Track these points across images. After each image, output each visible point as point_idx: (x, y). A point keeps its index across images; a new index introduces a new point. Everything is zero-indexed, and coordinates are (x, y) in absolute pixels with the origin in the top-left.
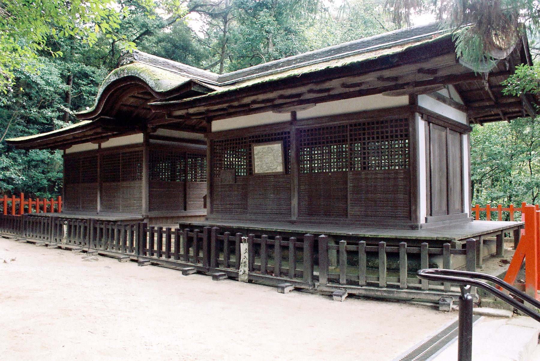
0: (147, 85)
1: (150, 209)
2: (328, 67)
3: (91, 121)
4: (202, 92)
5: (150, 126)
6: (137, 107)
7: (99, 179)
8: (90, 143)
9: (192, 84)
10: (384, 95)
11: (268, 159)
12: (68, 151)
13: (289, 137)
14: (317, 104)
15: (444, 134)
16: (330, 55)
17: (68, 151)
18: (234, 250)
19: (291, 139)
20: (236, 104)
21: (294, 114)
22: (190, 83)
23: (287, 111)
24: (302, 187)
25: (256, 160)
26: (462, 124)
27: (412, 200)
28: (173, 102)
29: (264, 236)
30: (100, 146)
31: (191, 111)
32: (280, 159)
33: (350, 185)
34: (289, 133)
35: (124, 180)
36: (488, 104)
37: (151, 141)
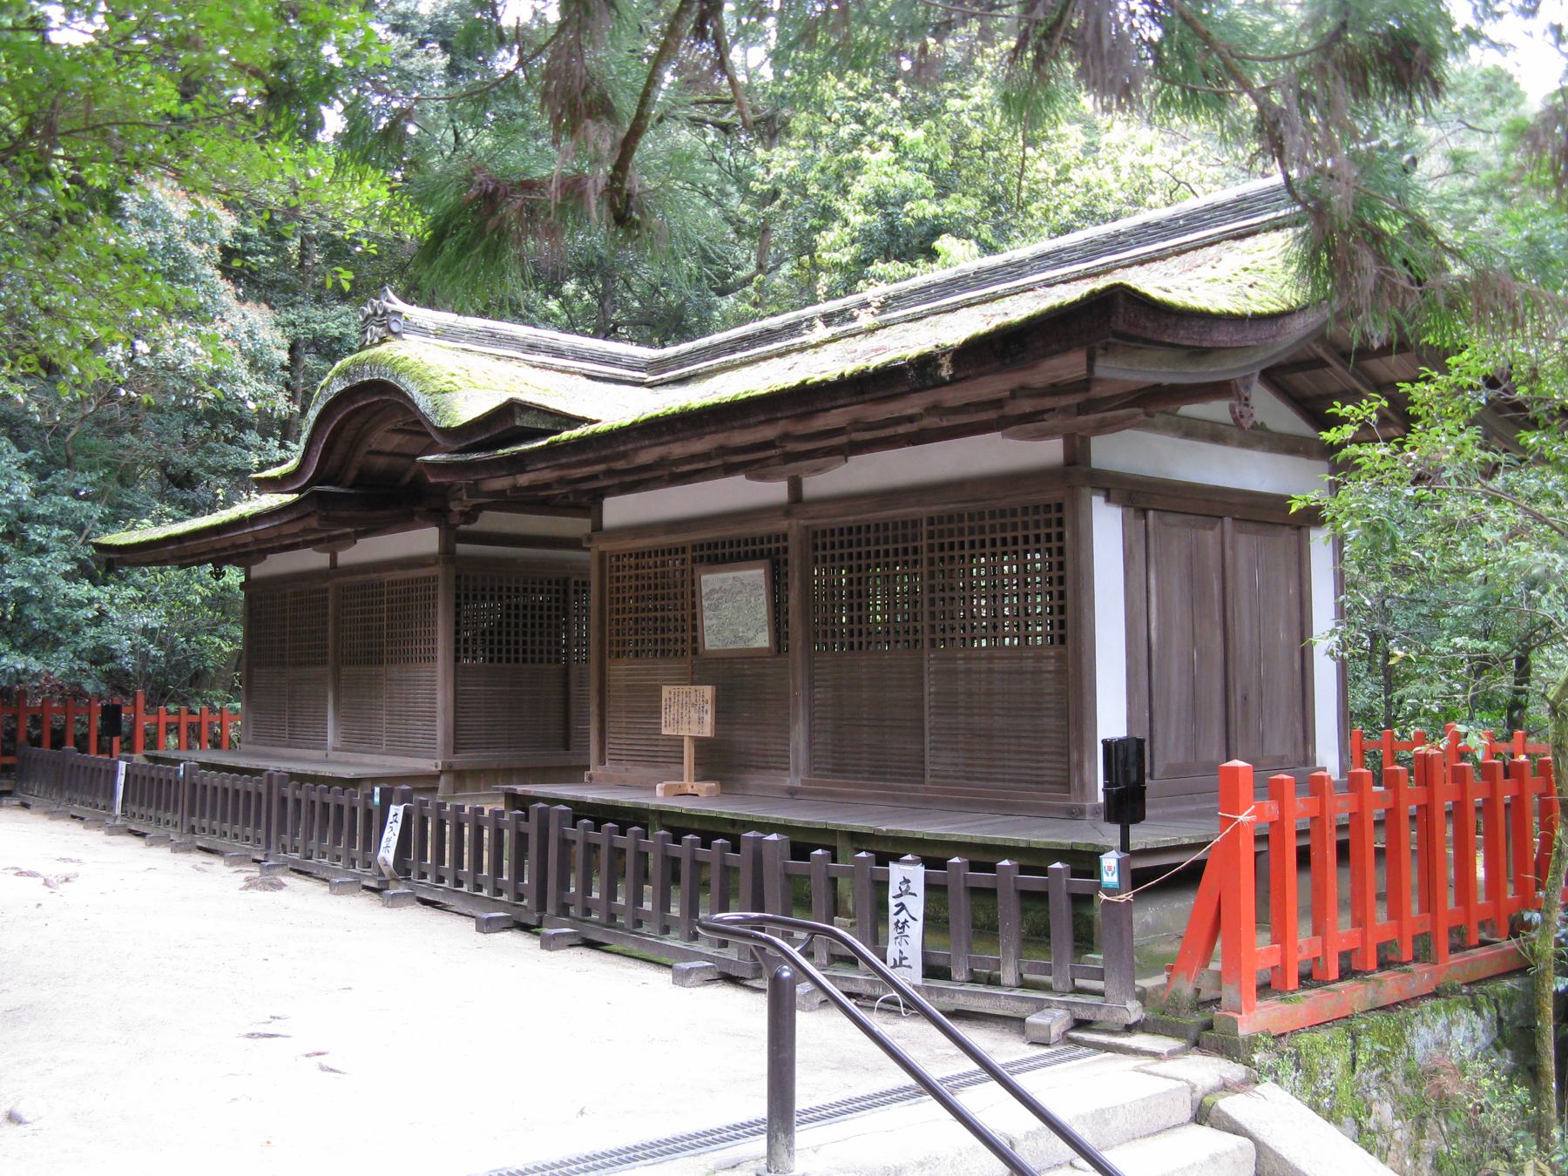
0: (416, 406)
1: (457, 747)
2: (804, 382)
3: (296, 496)
4: (549, 426)
5: (455, 507)
7: (330, 658)
9: (517, 410)
11: (735, 610)
12: (259, 570)
13: (786, 550)
14: (852, 459)
15: (1210, 537)
16: (927, 301)
17: (259, 570)
18: (374, 823)
19: (790, 556)
20: (621, 465)
21: (795, 486)
22: (511, 408)
24: (819, 694)
25: (706, 613)
27: (1073, 736)
28: (475, 456)
29: (956, 860)
30: (334, 559)
31: (1082, 267)
32: (763, 612)
33: (929, 688)
34: (785, 537)
35: (391, 661)
37: (463, 548)
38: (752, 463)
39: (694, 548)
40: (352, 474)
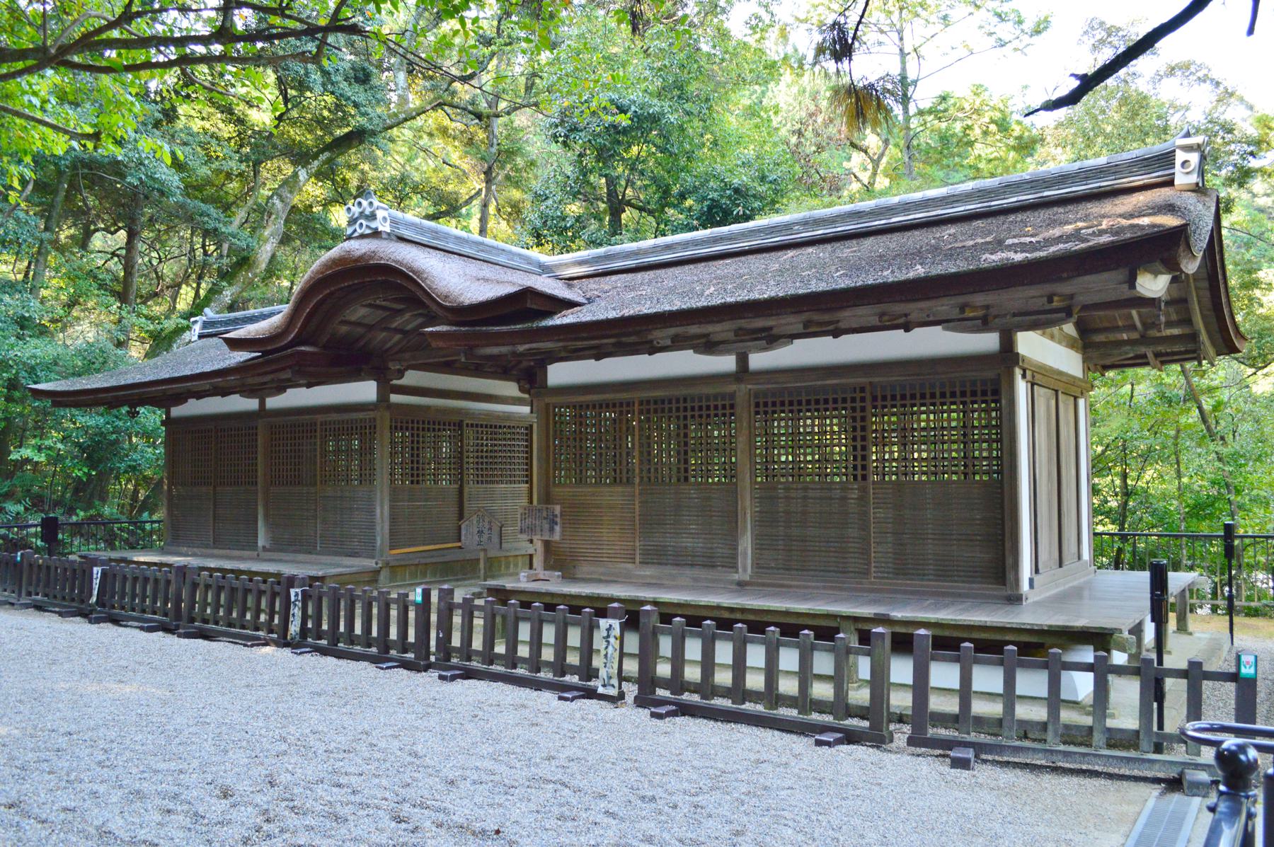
6: (370, 327)
8: (237, 396)
10: (945, 329)
12: (177, 411)
17: (177, 411)
21: (743, 360)
23: (728, 352)
26: (1074, 377)
30: (262, 403)
36: (1125, 336)
37: (395, 398)
38: (709, 346)
39: (641, 403)
40: (324, 339)
